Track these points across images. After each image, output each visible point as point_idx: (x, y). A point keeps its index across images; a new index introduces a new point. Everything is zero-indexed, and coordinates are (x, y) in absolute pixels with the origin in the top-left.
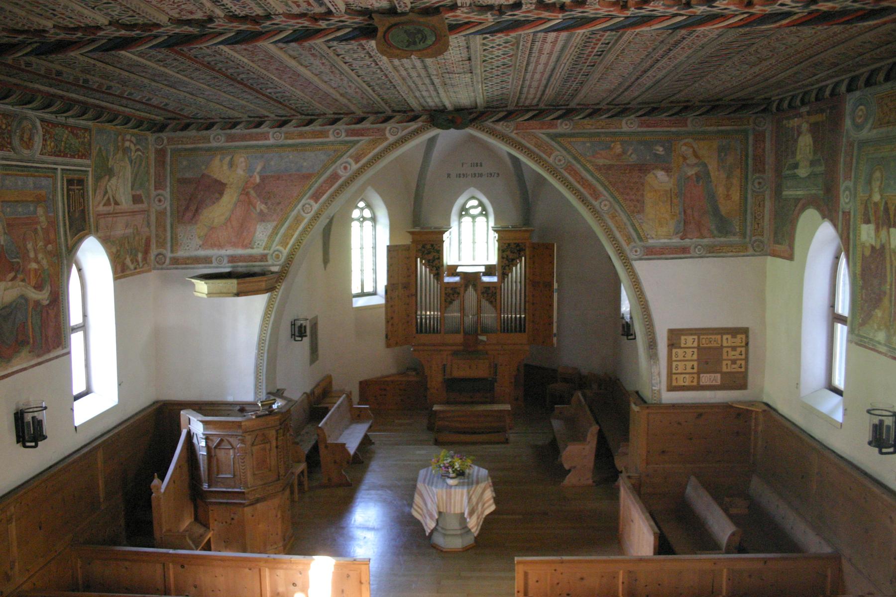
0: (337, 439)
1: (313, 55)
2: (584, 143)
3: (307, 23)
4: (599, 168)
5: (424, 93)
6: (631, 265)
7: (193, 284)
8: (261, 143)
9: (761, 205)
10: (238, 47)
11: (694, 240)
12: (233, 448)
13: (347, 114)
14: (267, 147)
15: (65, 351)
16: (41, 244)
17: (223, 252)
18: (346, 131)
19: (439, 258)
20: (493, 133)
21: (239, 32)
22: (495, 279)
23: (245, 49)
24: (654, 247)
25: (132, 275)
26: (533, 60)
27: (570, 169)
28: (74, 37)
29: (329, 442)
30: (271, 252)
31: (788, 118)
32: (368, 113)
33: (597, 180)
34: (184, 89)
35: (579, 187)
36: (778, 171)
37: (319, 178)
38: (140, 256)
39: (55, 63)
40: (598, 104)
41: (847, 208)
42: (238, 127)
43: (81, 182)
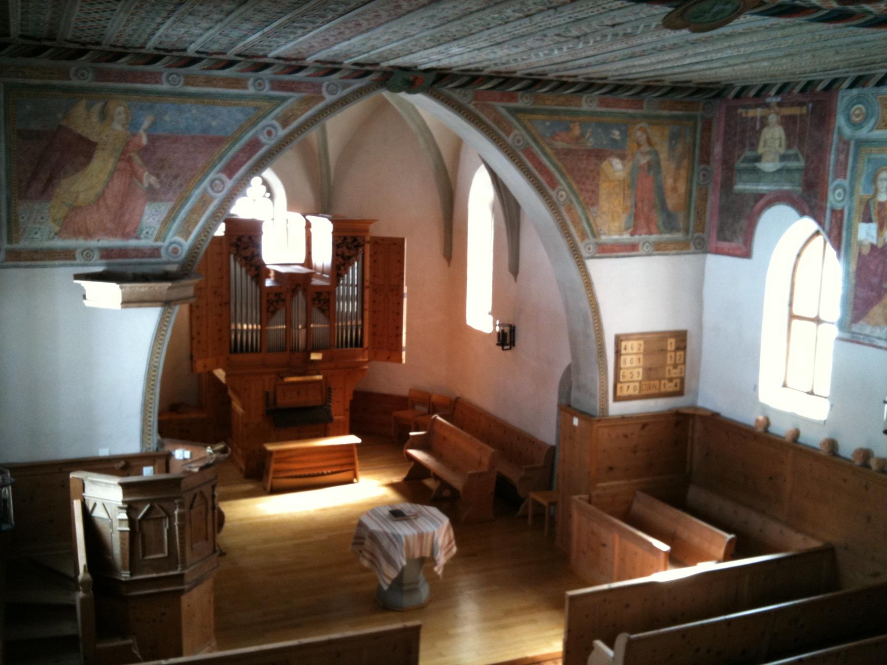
4: (557, 152)
7: (82, 289)
8: (148, 86)
11: (643, 236)
17: (93, 243)
18: (272, 82)
33: (555, 165)
35: (536, 172)
36: (728, 165)
37: (234, 144)
41: (839, 206)
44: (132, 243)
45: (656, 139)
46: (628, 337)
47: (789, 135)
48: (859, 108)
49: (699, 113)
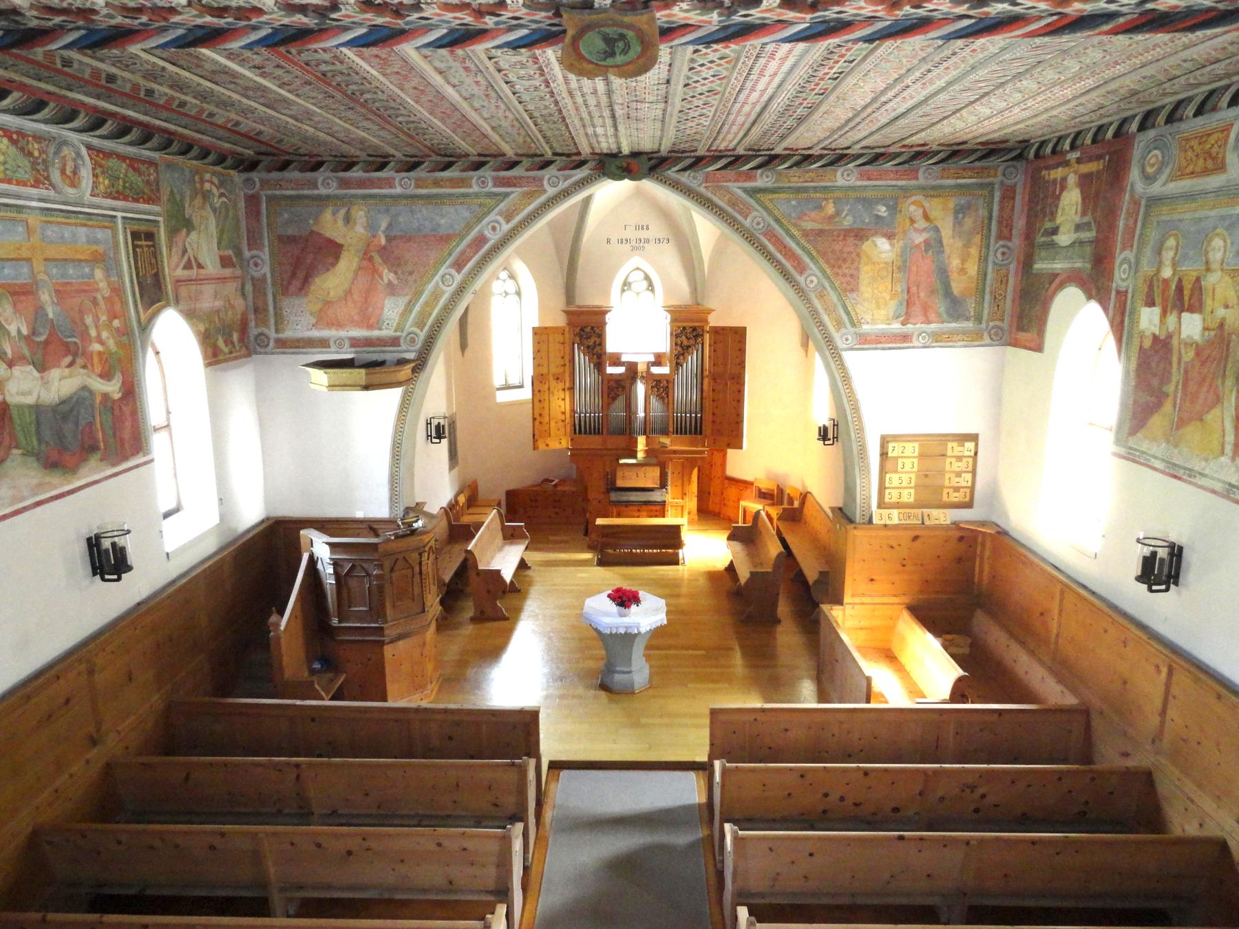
0: (489, 563)
1: (467, 69)
2: (789, 200)
3: (469, 19)
4: (806, 234)
5: (599, 130)
6: (840, 356)
9: (1004, 281)
10: (367, 51)
12: (368, 575)
13: (495, 156)
14: (392, 197)
15: (142, 460)
16: (104, 318)
17: (343, 333)
19: (600, 344)
20: (676, 186)
21: (374, 28)
22: (665, 370)
23: (377, 56)
24: (868, 334)
25: (226, 360)
26: (749, 84)
27: (770, 234)
28: (136, 22)
29: (480, 567)
30: (404, 334)
31: (1048, 168)
32: (522, 155)
33: (803, 248)
34: (286, 111)
36: (1029, 236)
37: (462, 240)
38: (235, 336)
39: (102, 63)
40: (809, 148)
42: (355, 169)
43: (150, 236)
44: (375, 333)
45: (934, 214)
46: (896, 438)
47: (1085, 198)
48: (1156, 156)
49: (997, 180)
